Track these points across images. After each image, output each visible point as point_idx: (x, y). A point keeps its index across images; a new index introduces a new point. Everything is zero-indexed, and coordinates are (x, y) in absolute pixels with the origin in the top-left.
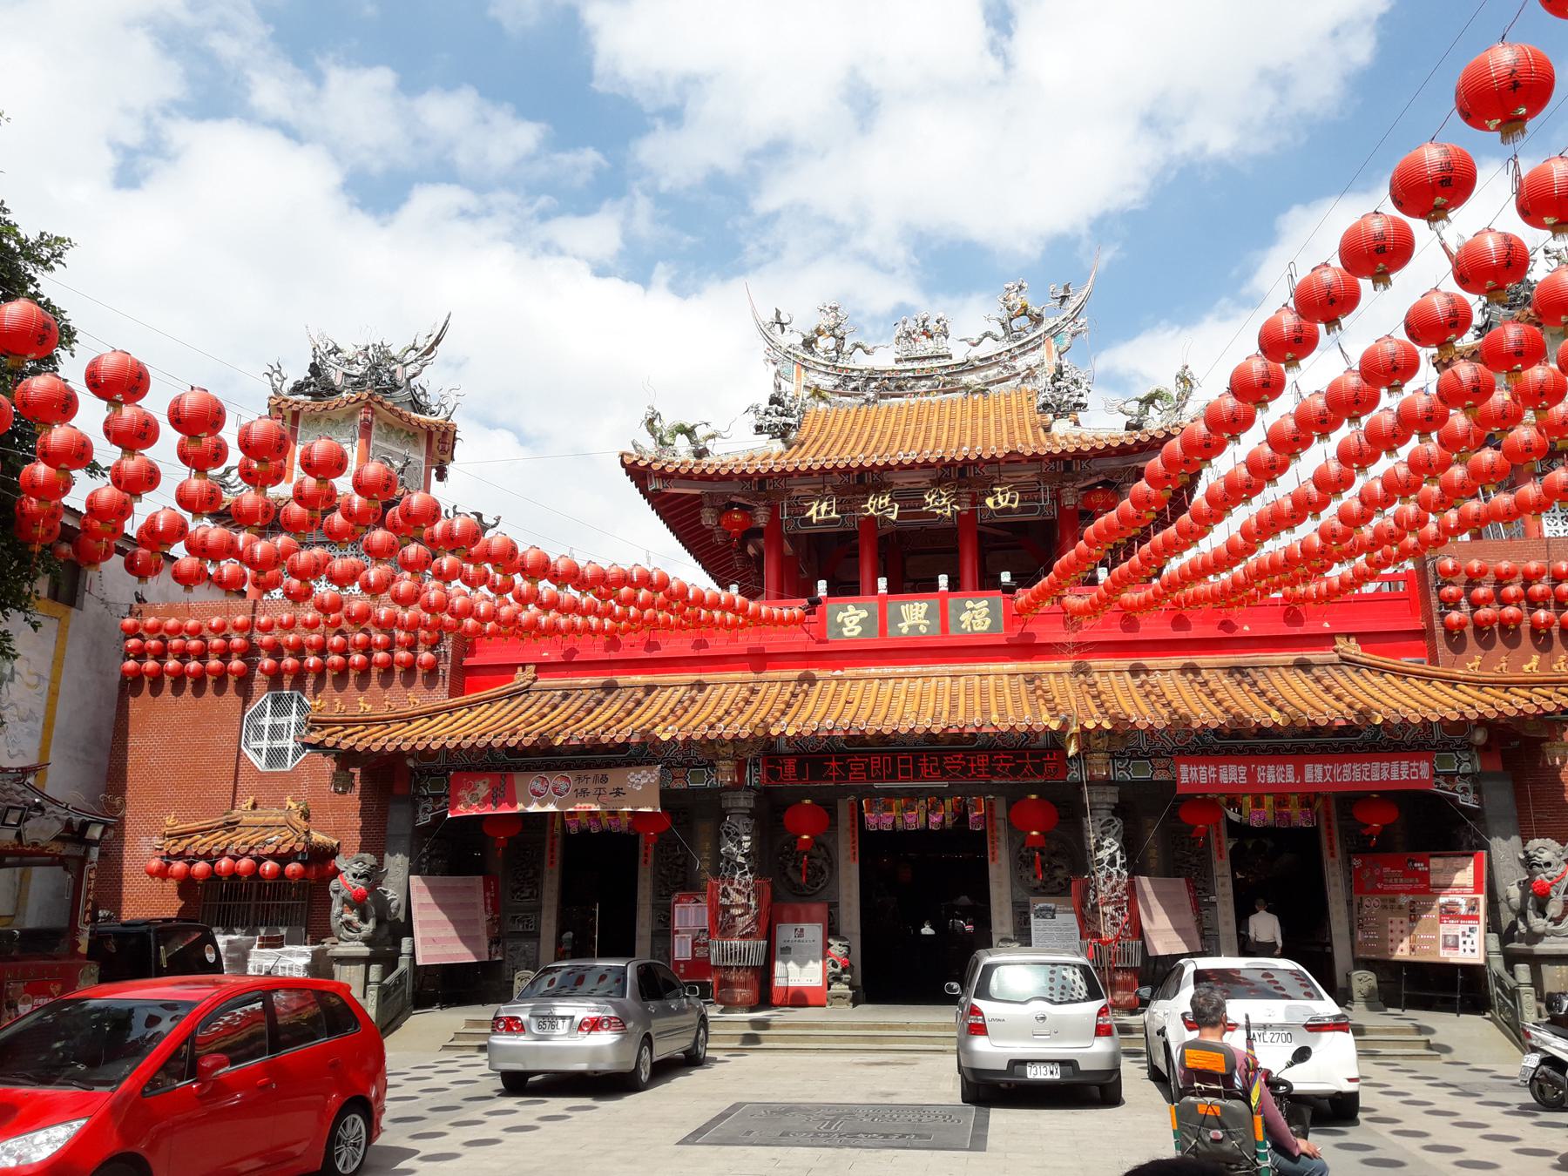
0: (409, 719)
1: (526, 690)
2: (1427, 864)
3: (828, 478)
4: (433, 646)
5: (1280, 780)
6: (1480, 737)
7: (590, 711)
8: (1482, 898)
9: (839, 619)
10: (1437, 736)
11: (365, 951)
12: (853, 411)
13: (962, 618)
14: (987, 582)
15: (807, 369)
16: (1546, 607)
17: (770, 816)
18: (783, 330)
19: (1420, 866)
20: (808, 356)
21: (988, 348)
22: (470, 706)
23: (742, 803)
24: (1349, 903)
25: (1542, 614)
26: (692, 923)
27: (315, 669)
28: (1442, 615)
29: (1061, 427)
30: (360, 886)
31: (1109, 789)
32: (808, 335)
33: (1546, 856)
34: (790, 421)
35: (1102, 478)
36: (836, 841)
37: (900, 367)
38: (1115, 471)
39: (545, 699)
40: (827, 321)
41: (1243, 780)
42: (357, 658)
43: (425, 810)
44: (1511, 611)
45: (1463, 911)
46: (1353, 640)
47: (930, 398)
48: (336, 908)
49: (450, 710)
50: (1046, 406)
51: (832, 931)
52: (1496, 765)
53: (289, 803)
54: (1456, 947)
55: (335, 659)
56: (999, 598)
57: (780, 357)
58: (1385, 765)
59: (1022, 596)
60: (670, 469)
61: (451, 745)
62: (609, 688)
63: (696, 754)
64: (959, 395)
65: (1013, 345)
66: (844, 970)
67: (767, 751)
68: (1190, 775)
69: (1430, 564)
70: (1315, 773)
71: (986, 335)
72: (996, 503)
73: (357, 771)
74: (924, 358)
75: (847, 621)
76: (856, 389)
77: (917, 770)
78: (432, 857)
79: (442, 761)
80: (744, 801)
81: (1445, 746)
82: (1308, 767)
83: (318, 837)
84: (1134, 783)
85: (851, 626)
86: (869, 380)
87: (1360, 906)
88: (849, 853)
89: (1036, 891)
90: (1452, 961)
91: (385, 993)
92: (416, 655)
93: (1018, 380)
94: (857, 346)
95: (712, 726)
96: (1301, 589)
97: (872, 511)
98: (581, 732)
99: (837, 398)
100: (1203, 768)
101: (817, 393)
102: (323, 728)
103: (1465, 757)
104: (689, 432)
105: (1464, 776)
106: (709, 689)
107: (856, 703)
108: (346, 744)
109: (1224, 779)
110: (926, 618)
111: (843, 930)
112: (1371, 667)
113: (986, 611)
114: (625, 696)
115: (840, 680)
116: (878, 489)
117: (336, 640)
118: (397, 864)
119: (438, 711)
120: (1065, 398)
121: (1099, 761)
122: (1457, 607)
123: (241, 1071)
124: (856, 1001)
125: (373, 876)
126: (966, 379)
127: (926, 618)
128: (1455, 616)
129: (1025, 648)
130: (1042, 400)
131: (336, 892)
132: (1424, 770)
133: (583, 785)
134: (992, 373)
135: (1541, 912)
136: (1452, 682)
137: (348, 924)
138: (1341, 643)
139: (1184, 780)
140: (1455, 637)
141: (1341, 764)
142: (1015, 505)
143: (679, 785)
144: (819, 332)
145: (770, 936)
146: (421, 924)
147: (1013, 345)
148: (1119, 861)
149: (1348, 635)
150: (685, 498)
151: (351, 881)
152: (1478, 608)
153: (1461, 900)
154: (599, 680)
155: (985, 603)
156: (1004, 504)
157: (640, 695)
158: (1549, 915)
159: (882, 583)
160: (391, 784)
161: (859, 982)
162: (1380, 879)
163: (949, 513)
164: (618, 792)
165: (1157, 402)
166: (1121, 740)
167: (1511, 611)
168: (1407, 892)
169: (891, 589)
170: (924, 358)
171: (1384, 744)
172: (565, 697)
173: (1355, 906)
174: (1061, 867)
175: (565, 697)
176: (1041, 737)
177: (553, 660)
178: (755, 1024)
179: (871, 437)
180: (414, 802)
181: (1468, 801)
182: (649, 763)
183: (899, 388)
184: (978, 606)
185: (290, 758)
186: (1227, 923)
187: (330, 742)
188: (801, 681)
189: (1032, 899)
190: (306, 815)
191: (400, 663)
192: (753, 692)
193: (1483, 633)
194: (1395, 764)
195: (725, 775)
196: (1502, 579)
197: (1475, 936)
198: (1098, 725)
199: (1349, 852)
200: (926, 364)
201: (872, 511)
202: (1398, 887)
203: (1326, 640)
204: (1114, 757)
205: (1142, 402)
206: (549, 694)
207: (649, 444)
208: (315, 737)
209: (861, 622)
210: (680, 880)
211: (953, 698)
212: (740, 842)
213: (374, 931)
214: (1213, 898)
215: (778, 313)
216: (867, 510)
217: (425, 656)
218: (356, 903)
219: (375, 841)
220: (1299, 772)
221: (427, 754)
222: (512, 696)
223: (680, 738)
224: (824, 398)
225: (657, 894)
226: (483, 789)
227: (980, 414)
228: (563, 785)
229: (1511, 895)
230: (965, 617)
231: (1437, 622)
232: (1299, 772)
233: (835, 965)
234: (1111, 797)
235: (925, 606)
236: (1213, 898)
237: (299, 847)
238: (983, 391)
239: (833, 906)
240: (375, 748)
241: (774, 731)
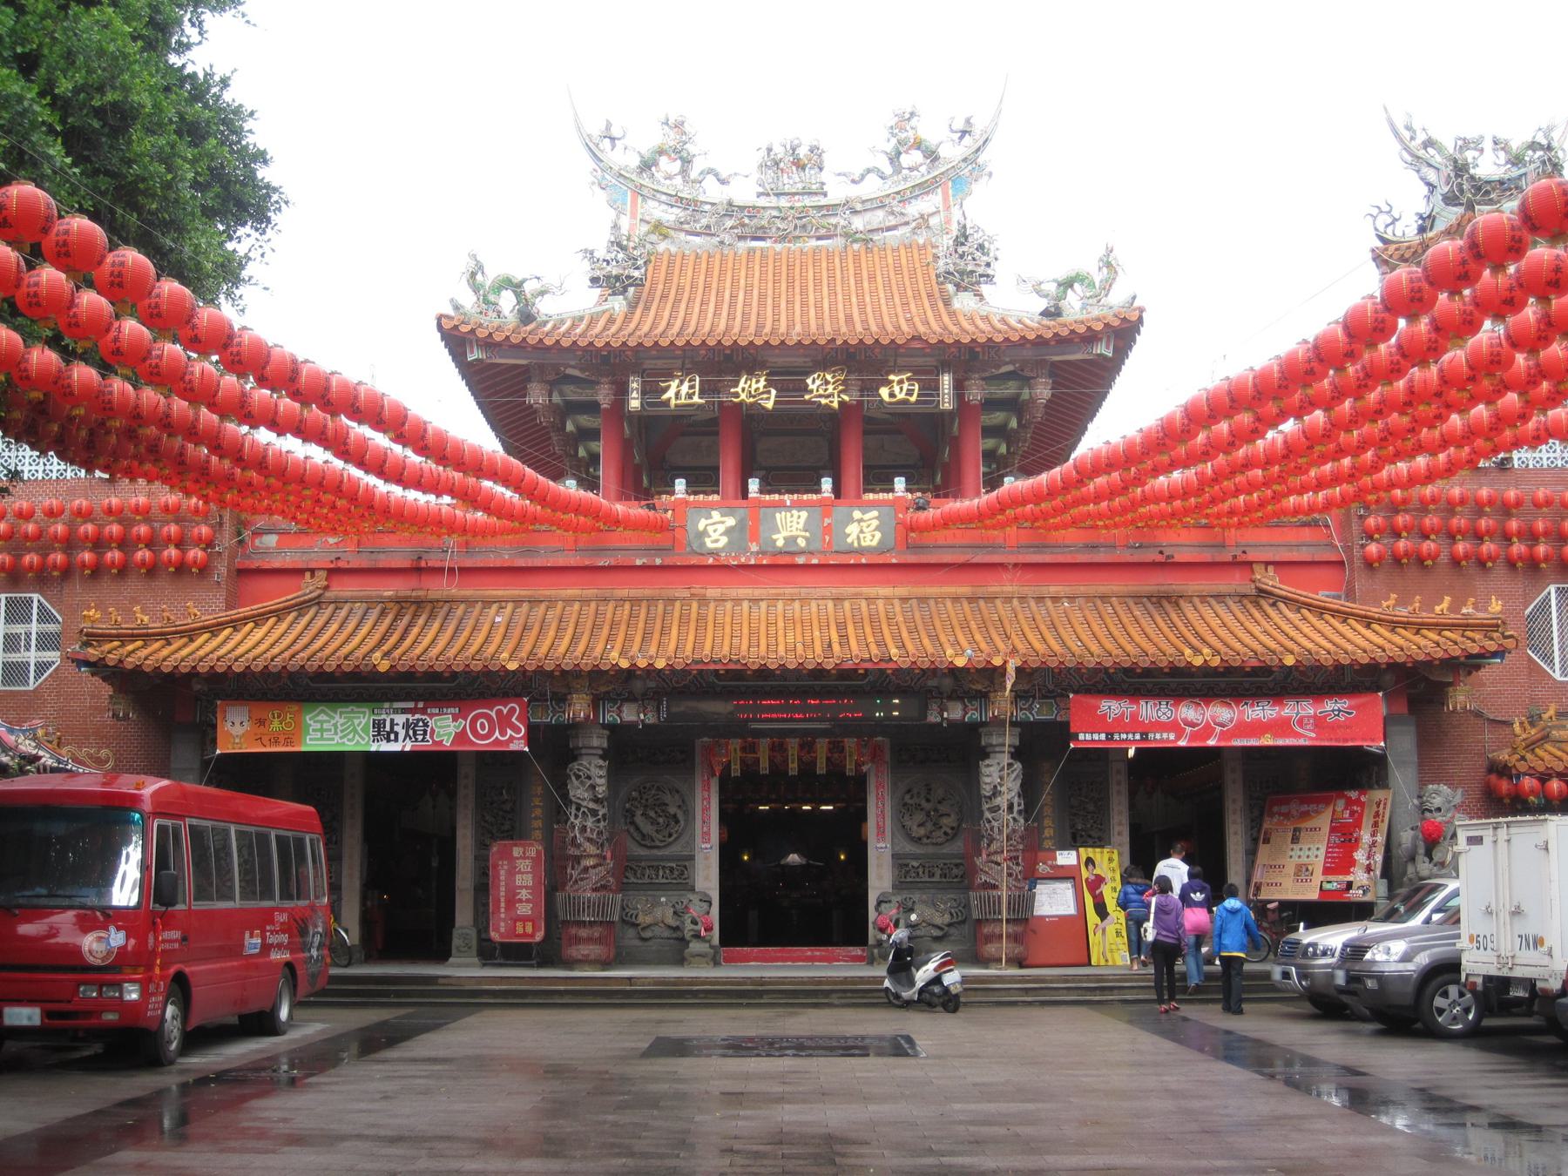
0: (191, 634)
9: (701, 527)
10: (1348, 679)
13: (848, 530)
18: (613, 147)
21: (872, 188)
23: (595, 742)
28: (1363, 546)
29: (964, 302)
32: (647, 155)
33: (1437, 801)
36: (692, 790)
37: (763, 202)
40: (671, 139)
57: (611, 179)
63: (537, 686)
64: (837, 243)
71: (869, 171)
72: (892, 395)
75: (710, 529)
84: (1037, 723)
85: (715, 536)
94: (710, 171)
99: (682, 235)
104: (517, 287)
113: (875, 523)
136: (1368, 621)
142: (913, 399)
144: (661, 152)
148: (1016, 808)
150: (501, 366)
156: (901, 396)
159: (754, 485)
160: (168, 706)
163: (835, 405)
165: (1076, 286)
179: (733, 297)
184: (866, 517)
201: (743, 396)
205: (1060, 285)
207: (468, 300)
208: (93, 653)
209: (728, 532)
212: (593, 787)
215: (609, 126)
216: (737, 395)
222: (301, 607)
227: (865, 275)
230: (852, 529)
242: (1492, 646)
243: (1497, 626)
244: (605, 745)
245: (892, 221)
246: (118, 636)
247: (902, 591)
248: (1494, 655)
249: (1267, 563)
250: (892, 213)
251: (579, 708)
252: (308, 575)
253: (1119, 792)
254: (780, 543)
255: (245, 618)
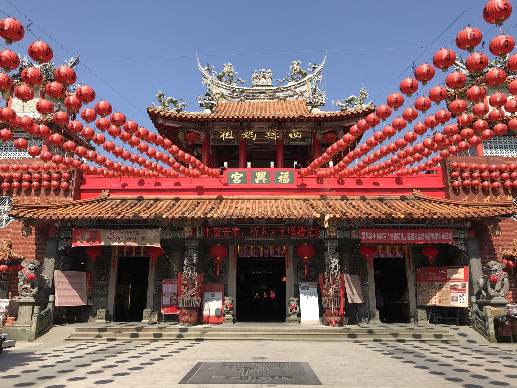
0: (56, 208)
1: (105, 199)
2: (446, 271)
3: (229, 123)
4: (68, 180)
5: (399, 239)
6: (468, 225)
7: (132, 207)
8: (467, 283)
9: (232, 177)
11: (33, 300)
12: (236, 103)
13: (279, 178)
14: (288, 165)
15: (219, 87)
16: (487, 181)
17: (205, 249)
19: (443, 272)
20: (220, 82)
22: (82, 204)
23: (193, 244)
24: (416, 285)
25: (486, 183)
26: (170, 291)
27: (16, 187)
28: (452, 182)
30: (32, 273)
31: (335, 241)
33: (496, 267)
34: (214, 102)
35: (331, 129)
38: (335, 127)
39: (113, 203)
41: (385, 238)
42: (35, 183)
43: (62, 244)
44: (475, 181)
45: (460, 288)
46: (419, 190)
47: (265, 100)
48: (21, 283)
49: (74, 205)
50: (310, 103)
51: (225, 294)
52: (472, 235)
53: (3, 241)
54: (457, 301)
55: (26, 183)
56: (294, 171)
58: (436, 234)
59: (303, 170)
60: (167, 115)
61: (74, 217)
62: (140, 199)
64: (275, 100)
65: (295, 83)
66: (230, 310)
67: (205, 223)
68: (366, 236)
69: (448, 164)
70: (411, 237)
72: (293, 136)
73: (33, 229)
74: (263, 86)
75: (235, 178)
76: (237, 95)
77: (255, 235)
78: (64, 263)
79: (69, 225)
80: (194, 244)
81: (455, 228)
82: (409, 234)
83: (15, 255)
85: (236, 180)
86: (242, 92)
87: (420, 286)
88: (233, 265)
89: (303, 280)
90: (455, 306)
91: (41, 318)
92: (60, 183)
93: (297, 96)
95: (183, 213)
96: (399, 171)
97: (246, 136)
98: (129, 214)
100: (371, 234)
101: (222, 96)
102: (18, 209)
103: (462, 232)
105: (461, 239)
106: (180, 202)
107: (239, 207)
108: (28, 216)
109: (378, 238)
110: (265, 177)
111: (229, 293)
112: (426, 200)
113: (288, 176)
114: (145, 203)
115: (232, 200)
116: (249, 128)
117: (26, 176)
118: (49, 263)
119: (69, 205)
120: (317, 100)
121: (333, 230)
122: (457, 180)
123: (436, 197)
124: (234, 322)
125: (38, 270)
126: (278, 94)
127: (265, 177)
128: (456, 183)
129: (302, 189)
130: (308, 101)
131: (21, 276)
132: (450, 235)
133: (129, 235)
134: (288, 93)
135: (493, 287)
136: (457, 205)
137: (26, 289)
138: (415, 192)
139: (364, 238)
140: (455, 190)
141: (421, 233)
142: (300, 137)
143: (167, 237)
145: (202, 296)
146: (58, 290)
147: (295, 83)
148: (338, 268)
149: (418, 189)
151: (28, 271)
152: (464, 180)
153: (459, 284)
154: (135, 197)
155: (288, 173)
157: (152, 202)
158: (496, 289)
159: (249, 164)
160: (49, 234)
161: (235, 314)
162: (428, 276)
163: (275, 139)
164: (143, 239)
166: (341, 223)
167: (475, 181)
168: (438, 281)
169: (252, 166)
170: (263, 86)
171: (434, 226)
172: (122, 202)
173: (418, 287)
174: (313, 271)
175: (122, 202)
176: (310, 221)
177: (117, 188)
178: (181, 330)
180: (57, 241)
181: (462, 248)
182: (156, 228)
183: (253, 96)
184: (285, 174)
185: (4, 223)
186: (372, 292)
187: (21, 214)
188: (217, 199)
189: (300, 283)
190: (10, 246)
191: (53, 186)
192: (198, 203)
193: (466, 189)
194: (440, 234)
195: (187, 233)
196: (472, 171)
197: (464, 297)
198: (334, 216)
199: (416, 267)
200: (264, 88)
201: (246, 136)
202: (434, 279)
203: (411, 190)
204: (339, 229)
206: (114, 201)
208: (15, 212)
209: (241, 178)
210: (166, 274)
211: (277, 207)
213: (38, 292)
214: (367, 283)
217: (64, 184)
218: (31, 281)
219: (40, 256)
220: (405, 236)
221: (63, 221)
223: (170, 217)
224: (225, 98)
225: (156, 280)
226: (87, 236)
228: (120, 235)
229: (480, 282)
230: (280, 178)
231: (450, 185)
232: (405, 236)
233: (227, 308)
234: (335, 244)
235: (265, 173)
236: (367, 283)
237: (6, 258)
238: (284, 99)
239: (227, 285)
240: (41, 217)
241: (209, 216)
242: (510, 212)
243: (511, 205)
244: (197, 245)
245: (292, 94)
246: (26, 207)
247: (297, 197)
248: (511, 215)
249: (418, 189)
250: (292, 91)
251: (187, 233)
252: (103, 191)
253: (113, 271)
254: (257, 182)
255: (78, 203)
